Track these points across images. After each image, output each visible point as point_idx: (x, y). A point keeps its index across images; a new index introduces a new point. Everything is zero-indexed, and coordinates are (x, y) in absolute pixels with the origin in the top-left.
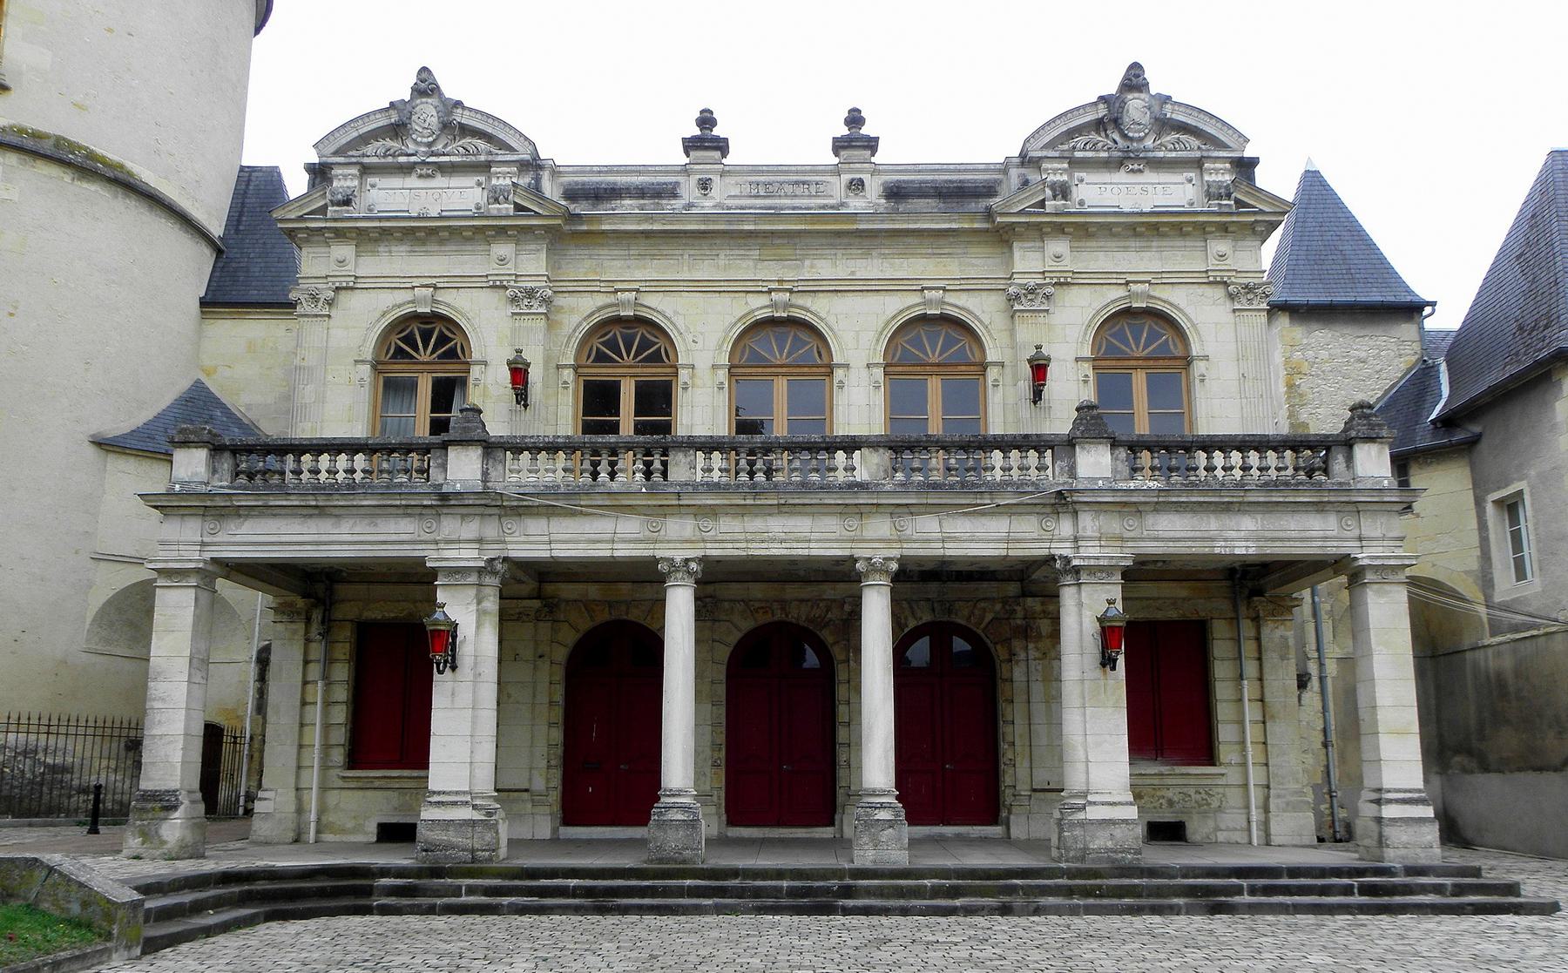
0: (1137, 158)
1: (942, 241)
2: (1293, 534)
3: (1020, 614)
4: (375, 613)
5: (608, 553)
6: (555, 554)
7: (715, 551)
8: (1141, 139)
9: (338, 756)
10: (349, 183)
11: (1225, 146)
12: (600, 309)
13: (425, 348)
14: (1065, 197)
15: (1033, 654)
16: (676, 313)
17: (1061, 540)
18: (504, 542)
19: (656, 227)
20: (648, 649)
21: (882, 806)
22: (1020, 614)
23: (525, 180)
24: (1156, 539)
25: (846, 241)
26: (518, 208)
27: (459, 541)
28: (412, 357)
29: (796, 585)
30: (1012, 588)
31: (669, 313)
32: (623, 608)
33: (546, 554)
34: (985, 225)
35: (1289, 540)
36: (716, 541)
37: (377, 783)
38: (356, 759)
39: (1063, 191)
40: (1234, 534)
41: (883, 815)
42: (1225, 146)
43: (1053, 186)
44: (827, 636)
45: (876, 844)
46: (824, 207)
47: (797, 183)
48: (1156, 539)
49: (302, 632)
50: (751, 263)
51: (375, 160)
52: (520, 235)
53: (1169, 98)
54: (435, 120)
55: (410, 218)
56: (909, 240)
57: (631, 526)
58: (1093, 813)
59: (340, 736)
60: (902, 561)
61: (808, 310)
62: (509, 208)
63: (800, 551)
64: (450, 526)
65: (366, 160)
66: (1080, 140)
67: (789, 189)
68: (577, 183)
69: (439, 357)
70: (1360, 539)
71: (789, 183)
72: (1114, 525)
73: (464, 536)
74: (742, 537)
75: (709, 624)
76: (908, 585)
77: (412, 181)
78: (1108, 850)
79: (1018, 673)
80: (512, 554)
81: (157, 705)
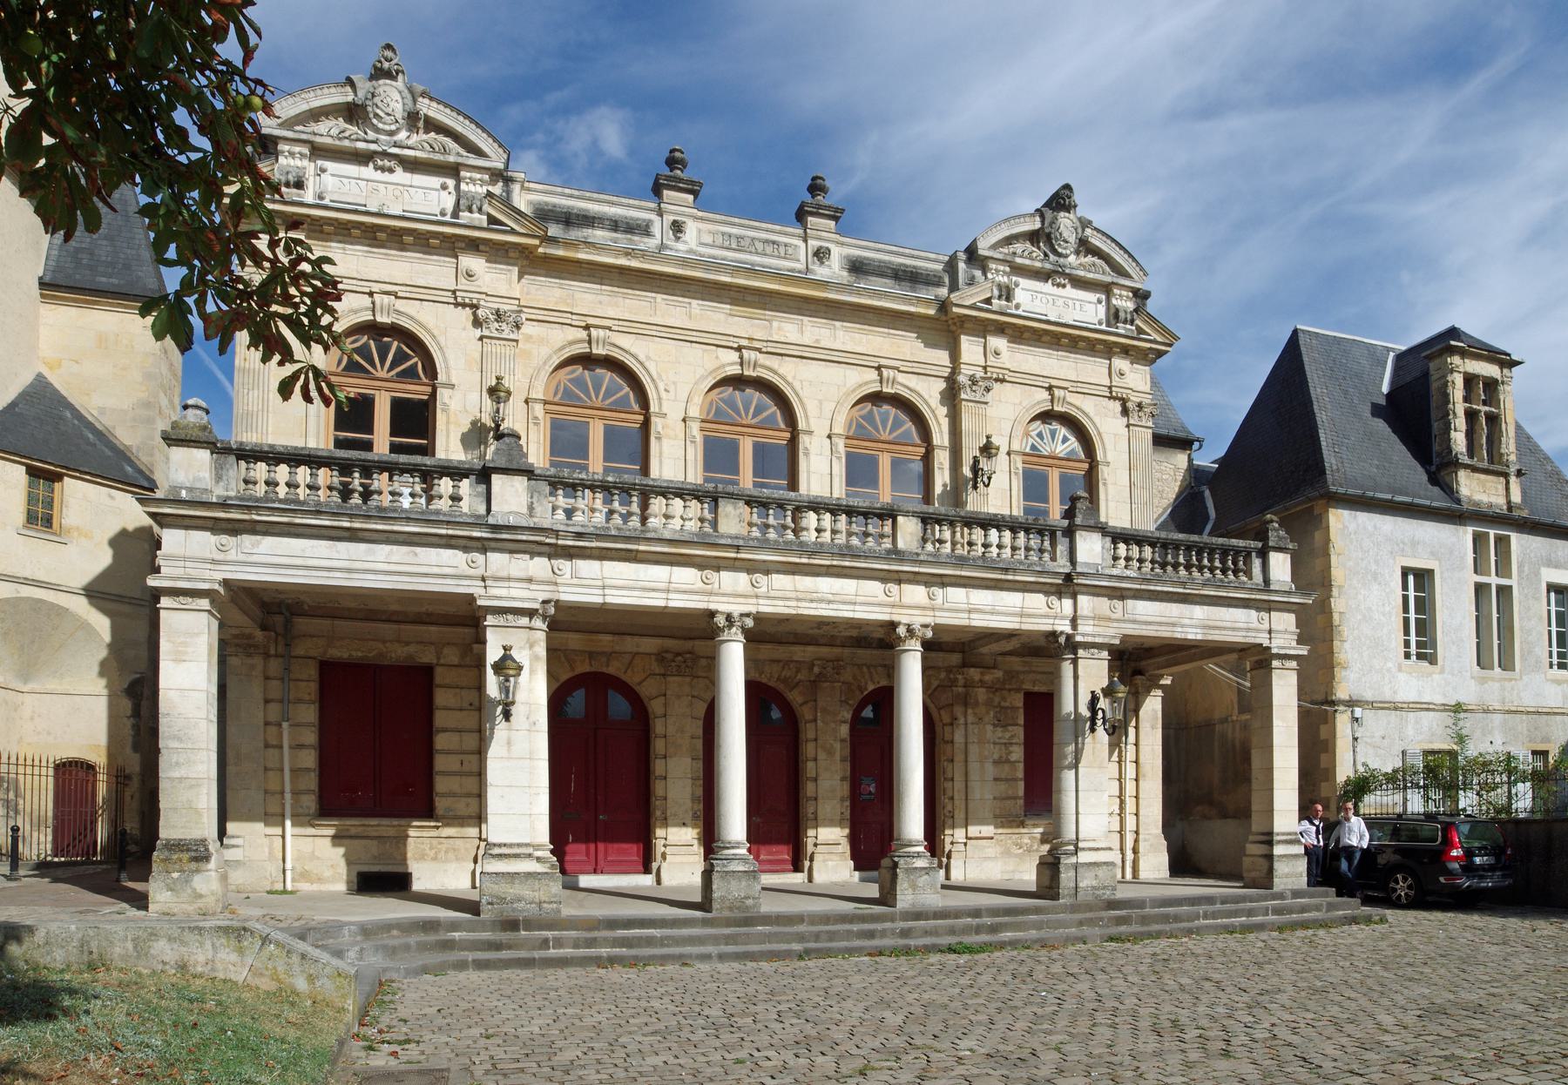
0: (1063, 274)
2: (1228, 625)
3: (961, 682)
4: (340, 652)
5: (662, 603)
6: (609, 600)
7: (767, 608)
8: (1066, 256)
10: (298, 163)
11: (1127, 275)
12: (571, 343)
13: (382, 363)
14: (1008, 299)
15: (970, 719)
16: (648, 358)
17: (1063, 618)
19: (635, 264)
20: (885, 701)
21: (919, 855)
22: (961, 682)
23: (497, 189)
24: (1134, 622)
25: (812, 307)
26: (492, 220)
27: (509, 579)
28: (367, 372)
29: (769, 646)
30: (955, 658)
31: (642, 357)
32: (604, 659)
33: (599, 600)
35: (1225, 628)
36: (768, 598)
39: (1007, 293)
40: (1187, 621)
41: (920, 863)
42: (1127, 275)
43: (999, 286)
44: (795, 697)
45: (914, 887)
46: (792, 270)
47: (766, 241)
48: (1134, 622)
49: (260, 667)
50: (722, 317)
51: (328, 141)
52: (498, 253)
53: (1090, 222)
54: (399, 107)
55: (367, 213)
58: (1084, 857)
59: (311, 781)
60: (937, 628)
61: (775, 372)
62: (483, 220)
64: (498, 561)
65: (318, 139)
66: (1019, 247)
67: (760, 246)
68: (547, 204)
69: (398, 375)
70: (483, 579)
71: (760, 240)
72: (1103, 604)
73: (515, 573)
74: (793, 595)
75: (688, 679)
76: (869, 652)
77: (368, 171)
78: (1094, 888)
79: (959, 737)
80: (564, 597)
81: (174, 744)
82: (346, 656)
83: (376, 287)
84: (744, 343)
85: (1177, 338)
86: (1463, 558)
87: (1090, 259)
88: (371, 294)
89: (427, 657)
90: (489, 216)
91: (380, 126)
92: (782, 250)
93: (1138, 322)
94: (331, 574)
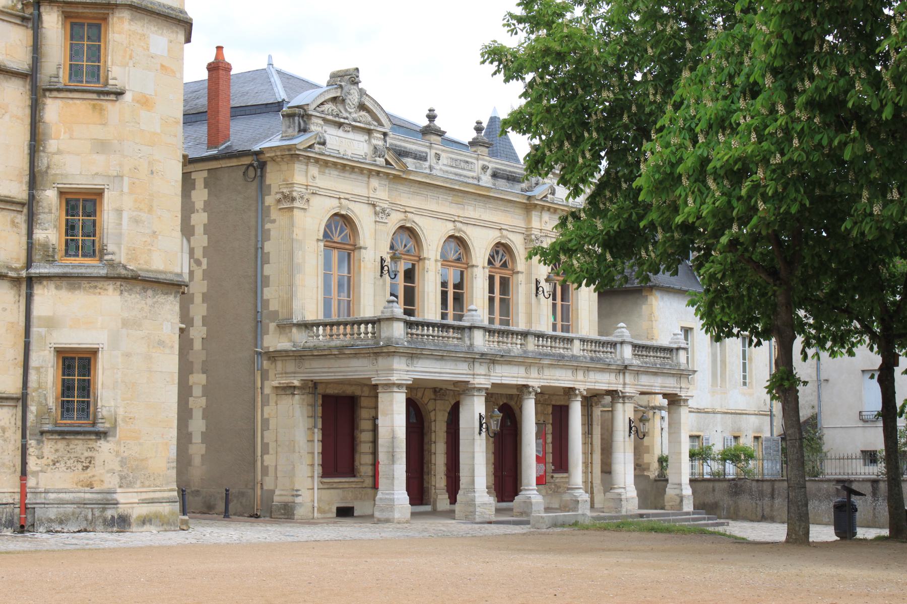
1: (509, 205)
9: (318, 470)
26: (387, 162)
34: (525, 201)
84: (456, 219)
87: (363, 113)
88: (340, 198)
89: (358, 393)
90: (386, 160)
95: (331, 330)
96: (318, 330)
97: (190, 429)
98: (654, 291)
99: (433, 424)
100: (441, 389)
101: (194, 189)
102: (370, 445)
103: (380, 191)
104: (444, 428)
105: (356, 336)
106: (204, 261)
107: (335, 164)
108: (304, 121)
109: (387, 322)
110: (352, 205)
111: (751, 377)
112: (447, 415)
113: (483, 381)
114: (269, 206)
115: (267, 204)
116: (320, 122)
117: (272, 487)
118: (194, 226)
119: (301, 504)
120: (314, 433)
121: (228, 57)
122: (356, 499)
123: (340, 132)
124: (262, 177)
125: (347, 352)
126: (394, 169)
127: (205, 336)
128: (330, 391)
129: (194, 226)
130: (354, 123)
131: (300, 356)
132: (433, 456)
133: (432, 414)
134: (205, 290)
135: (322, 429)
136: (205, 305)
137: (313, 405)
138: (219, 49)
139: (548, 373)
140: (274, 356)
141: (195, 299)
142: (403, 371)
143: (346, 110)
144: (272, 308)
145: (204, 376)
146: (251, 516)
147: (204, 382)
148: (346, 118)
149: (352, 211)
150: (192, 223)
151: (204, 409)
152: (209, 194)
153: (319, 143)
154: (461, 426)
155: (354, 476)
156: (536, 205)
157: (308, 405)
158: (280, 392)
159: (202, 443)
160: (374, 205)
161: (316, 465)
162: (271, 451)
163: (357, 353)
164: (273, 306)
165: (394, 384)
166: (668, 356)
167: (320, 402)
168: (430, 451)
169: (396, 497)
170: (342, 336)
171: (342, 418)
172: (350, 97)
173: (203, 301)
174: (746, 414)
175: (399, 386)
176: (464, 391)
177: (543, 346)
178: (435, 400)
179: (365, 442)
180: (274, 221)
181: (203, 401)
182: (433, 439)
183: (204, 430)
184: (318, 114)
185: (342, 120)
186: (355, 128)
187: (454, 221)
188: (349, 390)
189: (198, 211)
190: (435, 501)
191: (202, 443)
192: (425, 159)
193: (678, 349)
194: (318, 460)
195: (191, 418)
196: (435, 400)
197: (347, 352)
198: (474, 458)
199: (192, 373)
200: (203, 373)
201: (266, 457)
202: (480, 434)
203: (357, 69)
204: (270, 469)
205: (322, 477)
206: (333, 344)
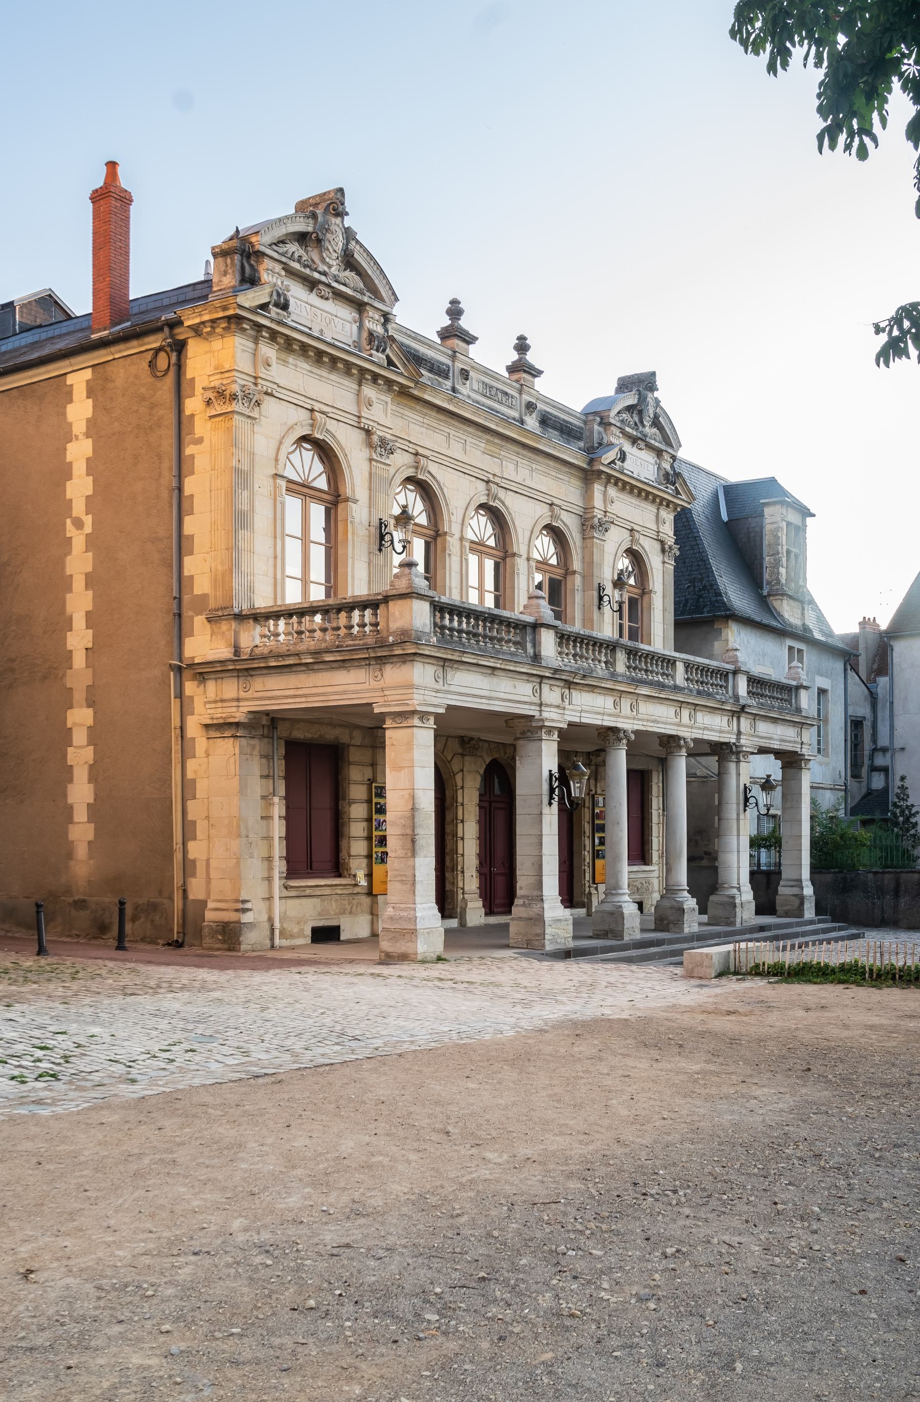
9: (279, 867)
11: (382, 300)
18: (564, 709)
26: (390, 363)
34: (585, 466)
37: (308, 892)
38: (292, 872)
42: (382, 300)
55: (309, 335)
56: (551, 463)
57: (605, 702)
63: (772, 746)
82: (302, 737)
83: (317, 406)
85: (694, 499)
86: (784, 667)
88: (312, 410)
89: (345, 739)
90: (388, 357)
91: (327, 260)
92: (493, 393)
93: (388, 351)
94: (491, 702)
95: (300, 623)
96: (276, 625)
97: (70, 801)
98: (730, 622)
99: (460, 792)
100: (472, 739)
101: (71, 401)
102: (364, 824)
103: (382, 411)
104: (476, 799)
105: (343, 632)
106: (88, 520)
107: (304, 347)
108: (251, 266)
109: (400, 602)
110: (332, 425)
111: (827, 743)
112: (479, 779)
113: (554, 716)
114: (192, 416)
115: (188, 412)
116: (278, 268)
117: (201, 896)
118: (71, 463)
119: (251, 925)
120: (271, 804)
121: (125, 181)
122: (343, 912)
123: (313, 298)
124: (180, 367)
125: (329, 658)
126: (401, 374)
127: (90, 645)
128: (299, 734)
129: (71, 463)
130: (335, 284)
131: (244, 667)
132: (460, 843)
133: (459, 778)
134: (90, 569)
135: (287, 798)
136: (90, 593)
137: (267, 757)
138: (112, 166)
139: (646, 708)
140: (205, 672)
141: (74, 585)
142: (427, 688)
143: (323, 261)
144: (197, 591)
145: (90, 712)
146: (169, 944)
147: (90, 722)
148: (324, 274)
149: (334, 437)
150: (69, 458)
151: (91, 766)
152: (95, 407)
153: (277, 305)
154: (519, 791)
155: (340, 876)
156: (601, 472)
157: (262, 756)
158: (213, 734)
159: (89, 822)
160: (368, 432)
161: (277, 858)
162: (200, 834)
163: (347, 658)
164: (202, 586)
165: (414, 712)
166: (786, 697)
167: (282, 751)
168: (455, 835)
169: (418, 914)
170: (318, 634)
171: (320, 767)
172: (329, 236)
173: (87, 587)
174: (822, 788)
175: (423, 715)
176: (523, 733)
177: (635, 669)
178: (463, 755)
179: (357, 820)
180: (200, 441)
181: (88, 754)
182: (460, 817)
183: (92, 801)
184: (275, 255)
185: (316, 275)
186: (339, 295)
187: (488, 482)
188: (331, 734)
189: (77, 438)
190: (464, 910)
191: (89, 822)
192: (447, 377)
193: (798, 688)
194: (279, 849)
195: (71, 780)
196: (463, 755)
197: (329, 658)
198: (541, 844)
199: (71, 707)
200: (89, 706)
201: (191, 845)
202: (550, 804)
203: (341, 190)
204: (198, 864)
205: (287, 878)
206: (302, 647)
